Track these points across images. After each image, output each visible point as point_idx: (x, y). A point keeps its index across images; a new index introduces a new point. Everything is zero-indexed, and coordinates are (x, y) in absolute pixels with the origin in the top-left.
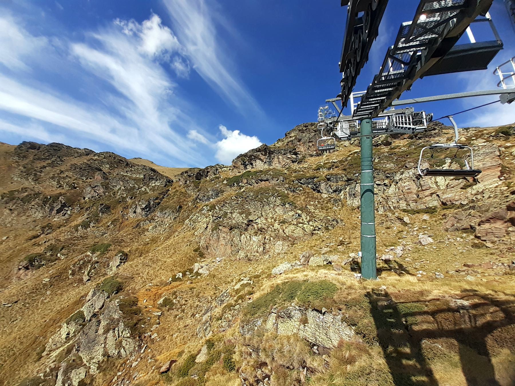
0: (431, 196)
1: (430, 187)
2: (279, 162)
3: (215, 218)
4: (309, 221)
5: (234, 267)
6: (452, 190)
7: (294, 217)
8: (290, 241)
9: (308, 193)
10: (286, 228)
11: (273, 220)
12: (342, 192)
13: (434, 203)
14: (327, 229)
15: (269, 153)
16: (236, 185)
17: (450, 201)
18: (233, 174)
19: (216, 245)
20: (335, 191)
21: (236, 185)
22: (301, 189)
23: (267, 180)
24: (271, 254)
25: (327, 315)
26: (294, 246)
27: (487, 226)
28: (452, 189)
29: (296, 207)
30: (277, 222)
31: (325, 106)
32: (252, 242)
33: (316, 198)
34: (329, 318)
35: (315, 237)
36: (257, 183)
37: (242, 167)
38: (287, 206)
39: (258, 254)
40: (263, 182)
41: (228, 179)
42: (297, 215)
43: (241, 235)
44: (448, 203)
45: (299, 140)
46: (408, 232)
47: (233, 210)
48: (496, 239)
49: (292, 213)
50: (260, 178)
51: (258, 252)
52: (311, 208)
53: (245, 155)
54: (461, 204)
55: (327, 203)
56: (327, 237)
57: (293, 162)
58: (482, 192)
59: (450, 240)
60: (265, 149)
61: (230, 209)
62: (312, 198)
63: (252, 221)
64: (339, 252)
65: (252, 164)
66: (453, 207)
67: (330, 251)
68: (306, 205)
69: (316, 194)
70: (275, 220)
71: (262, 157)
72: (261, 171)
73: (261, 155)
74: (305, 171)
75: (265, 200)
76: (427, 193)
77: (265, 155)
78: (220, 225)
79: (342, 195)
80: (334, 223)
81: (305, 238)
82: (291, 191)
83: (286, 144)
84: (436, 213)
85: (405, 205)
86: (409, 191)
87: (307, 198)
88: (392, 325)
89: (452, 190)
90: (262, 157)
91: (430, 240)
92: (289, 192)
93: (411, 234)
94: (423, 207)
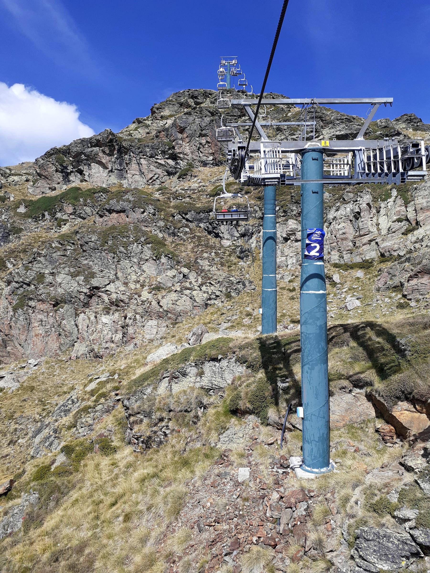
0: (370, 244)
1: (370, 232)
2: (142, 173)
3: (17, 285)
4: (202, 285)
5: (69, 372)
6: (392, 236)
7: (176, 279)
8: (170, 318)
9: (199, 237)
10: (163, 297)
11: (138, 286)
12: (254, 237)
13: (371, 254)
14: (228, 296)
15: (119, 151)
16: (47, 216)
17: (389, 251)
18: (38, 191)
19: (23, 337)
20: (243, 235)
21: (47, 216)
22: (187, 230)
23: (123, 211)
24: (138, 343)
25: (223, 361)
26: (177, 326)
27: (414, 282)
28: (393, 234)
29: (178, 262)
30: (147, 288)
31: (232, 59)
32: (100, 326)
33: (212, 247)
34: (224, 363)
35: (210, 310)
36: (101, 216)
37: (59, 177)
38: (164, 260)
39: (112, 345)
40: (114, 215)
41: (29, 204)
42: (182, 275)
43: (77, 315)
44: (387, 254)
45: (182, 131)
46: (335, 295)
47: (56, 267)
48: (421, 297)
49: (172, 273)
50: (107, 206)
51: (113, 342)
52: (204, 264)
53: (65, 151)
54: (398, 255)
55: (230, 255)
56: (228, 307)
57: (169, 174)
58: (422, 240)
59: (379, 302)
60: (111, 141)
61: (50, 266)
62: (207, 246)
63: (97, 288)
64: (244, 326)
65: (81, 172)
66: (391, 259)
67: (232, 326)
68: (197, 259)
69: (213, 241)
70: (143, 286)
71: (105, 159)
72: (104, 191)
73: (101, 154)
74: (194, 196)
75: (122, 249)
76: (366, 239)
77: (111, 154)
78: (31, 299)
79: (253, 242)
80: (240, 286)
81: (195, 312)
82: (169, 234)
83: (154, 133)
84: (373, 268)
85: (337, 257)
86: (344, 236)
87: (198, 246)
88: (274, 353)
89: (392, 236)
90: (105, 159)
91: (358, 303)
92: (166, 236)
93: (339, 297)
94: (358, 260)
